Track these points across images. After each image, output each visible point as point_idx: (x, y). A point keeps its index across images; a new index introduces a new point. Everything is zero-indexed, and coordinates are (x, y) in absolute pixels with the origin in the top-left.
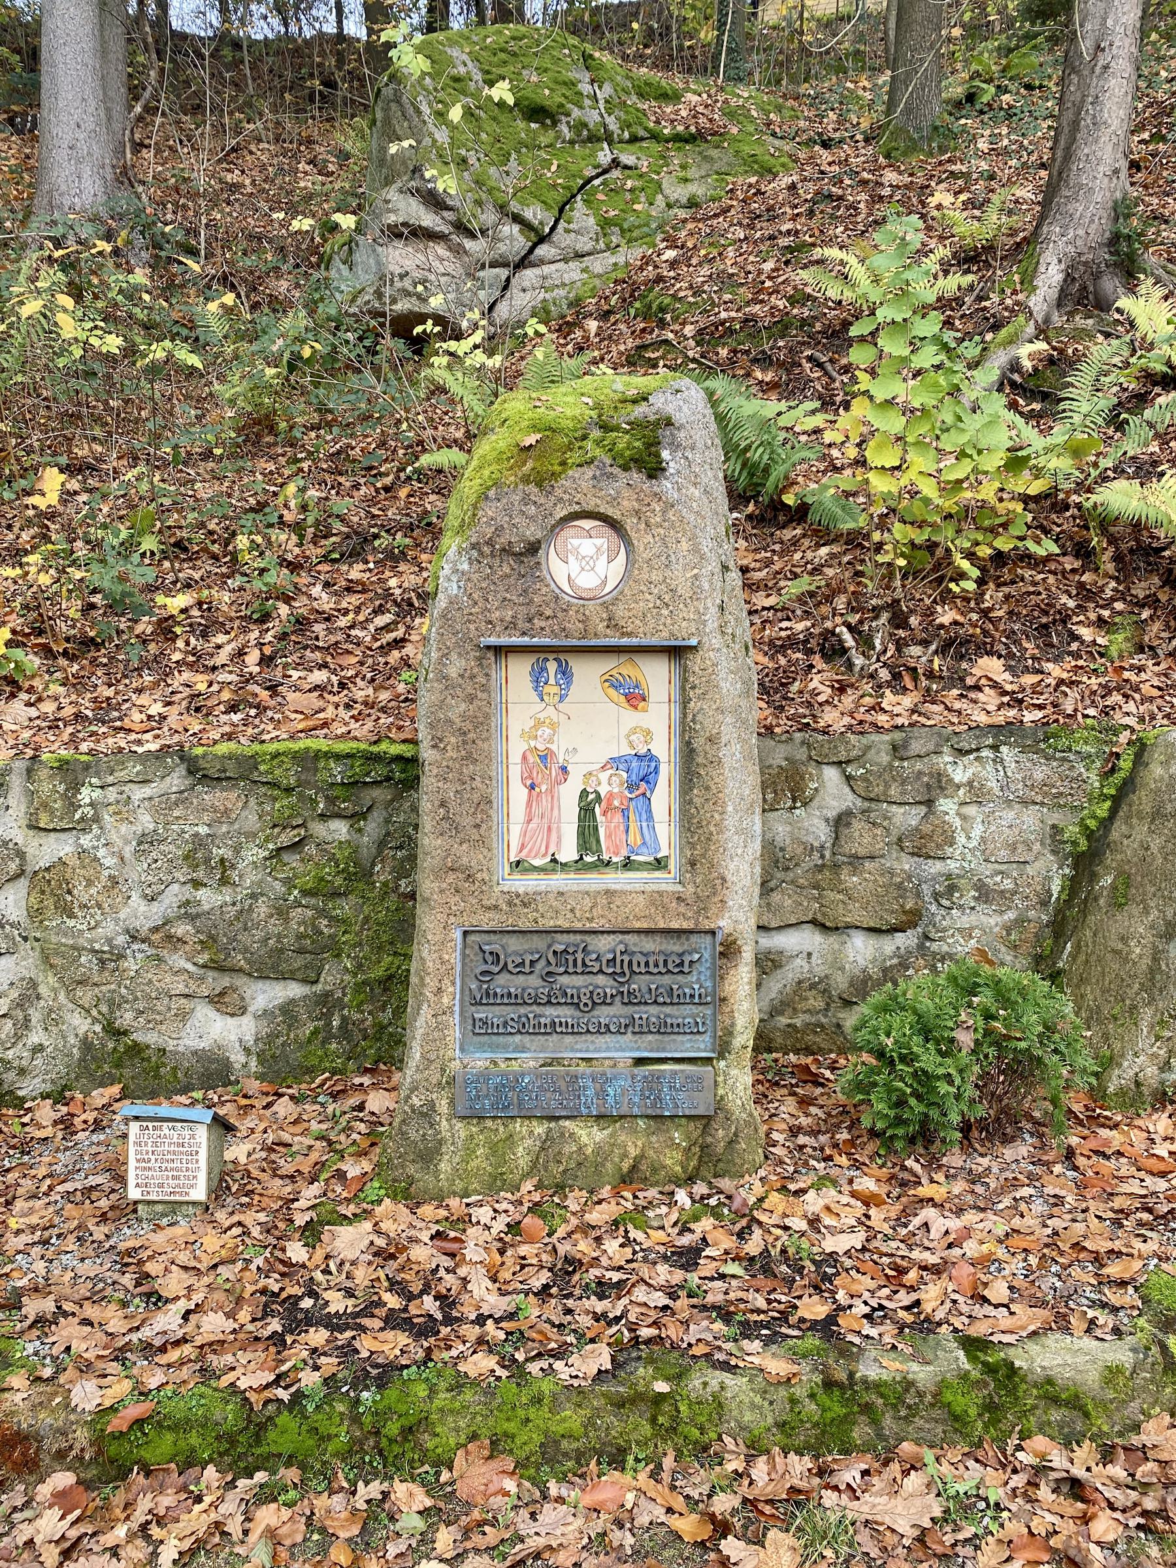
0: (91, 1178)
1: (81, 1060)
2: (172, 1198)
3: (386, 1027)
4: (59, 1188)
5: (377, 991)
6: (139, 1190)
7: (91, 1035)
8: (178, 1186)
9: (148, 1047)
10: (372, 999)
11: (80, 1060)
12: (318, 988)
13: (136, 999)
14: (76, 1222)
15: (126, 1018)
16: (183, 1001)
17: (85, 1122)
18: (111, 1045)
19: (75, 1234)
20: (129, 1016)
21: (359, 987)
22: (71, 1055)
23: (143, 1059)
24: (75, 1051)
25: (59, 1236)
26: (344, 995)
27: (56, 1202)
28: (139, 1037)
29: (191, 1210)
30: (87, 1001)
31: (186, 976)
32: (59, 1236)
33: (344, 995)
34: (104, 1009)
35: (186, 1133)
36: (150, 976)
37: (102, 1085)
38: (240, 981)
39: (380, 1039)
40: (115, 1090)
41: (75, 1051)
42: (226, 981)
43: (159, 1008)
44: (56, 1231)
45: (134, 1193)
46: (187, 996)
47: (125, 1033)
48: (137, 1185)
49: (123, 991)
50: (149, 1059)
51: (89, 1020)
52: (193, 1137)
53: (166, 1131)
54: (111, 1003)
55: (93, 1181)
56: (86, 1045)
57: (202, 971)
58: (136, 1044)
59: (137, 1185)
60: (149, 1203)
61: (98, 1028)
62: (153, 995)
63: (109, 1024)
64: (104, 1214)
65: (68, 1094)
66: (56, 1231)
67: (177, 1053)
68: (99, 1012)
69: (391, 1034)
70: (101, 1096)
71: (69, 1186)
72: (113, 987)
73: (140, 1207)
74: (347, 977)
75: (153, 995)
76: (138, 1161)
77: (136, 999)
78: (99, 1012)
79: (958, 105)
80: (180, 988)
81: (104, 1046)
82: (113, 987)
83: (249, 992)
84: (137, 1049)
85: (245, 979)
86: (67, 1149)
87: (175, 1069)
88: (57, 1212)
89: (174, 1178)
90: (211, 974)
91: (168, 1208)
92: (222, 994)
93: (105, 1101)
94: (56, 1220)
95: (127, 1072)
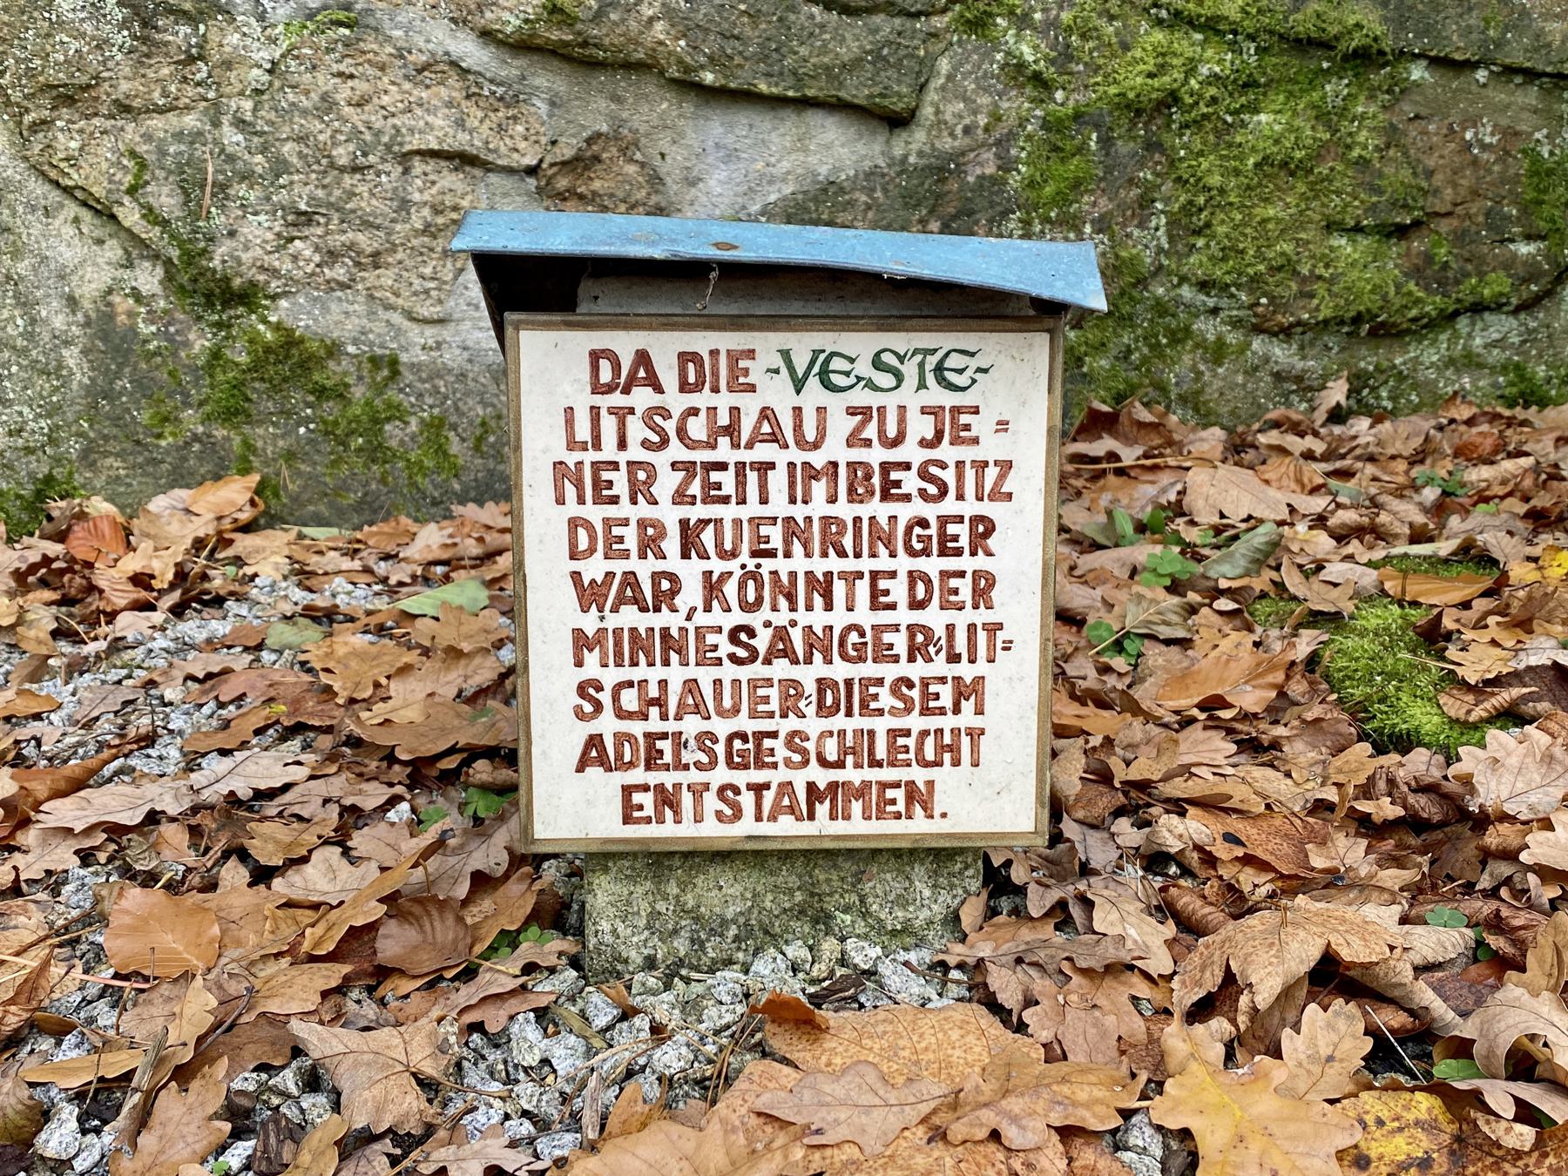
0: (215, 765)
1: (98, 393)
2: (824, 826)
3: (1141, 282)
4: (64, 812)
5: (1123, 147)
6: (605, 785)
7: (123, 304)
8: (860, 749)
9: (334, 350)
10: (1111, 174)
11: (90, 391)
12: (913, 144)
13: (280, 167)
14: (197, 1008)
15: (248, 240)
16: (450, 180)
17: (141, 580)
18: (200, 342)
19: (208, 1093)
20: (259, 230)
21: (1059, 134)
22: (56, 370)
23: (321, 392)
24: (72, 357)
25: (97, 1104)
26: (1007, 166)
27: (54, 882)
28: (296, 313)
29: (928, 900)
30: (99, 170)
31: (453, 89)
32: (97, 1104)
33: (1007, 166)
34: (166, 199)
35: (912, 400)
36: (324, 81)
37: (181, 478)
38: (651, 112)
39: (1126, 321)
40: (234, 494)
41: (72, 357)
42: (594, 111)
43: (366, 204)
44: (68, 1064)
45: (571, 805)
46: (464, 160)
47: (247, 297)
48: (593, 754)
49: (232, 137)
50: (340, 394)
51: (113, 250)
52: (951, 426)
53: (777, 394)
54: (190, 184)
55: (227, 776)
56: (109, 338)
57: (510, 69)
58: (289, 341)
59: (593, 754)
60: (658, 862)
61: (148, 279)
62: (342, 155)
63: (190, 257)
64: (360, 936)
65: (57, 507)
66: (68, 1064)
67: (437, 373)
68: (150, 215)
69: (1160, 308)
70: (177, 519)
71: (116, 803)
72: (191, 121)
73: (603, 894)
74: (1016, 104)
75: (342, 155)
76: (589, 595)
77: (280, 167)
78: (150, 215)
79: (286, 617)
80: (438, 130)
81: (176, 344)
82: (191, 121)
83: (677, 156)
84: (293, 359)
85: (665, 105)
86: (77, 667)
87: (435, 427)
88: (67, 938)
89: (831, 699)
90: (546, 80)
91: (771, 894)
92: (581, 164)
93: (203, 527)
94: (67, 985)
95: (268, 437)
